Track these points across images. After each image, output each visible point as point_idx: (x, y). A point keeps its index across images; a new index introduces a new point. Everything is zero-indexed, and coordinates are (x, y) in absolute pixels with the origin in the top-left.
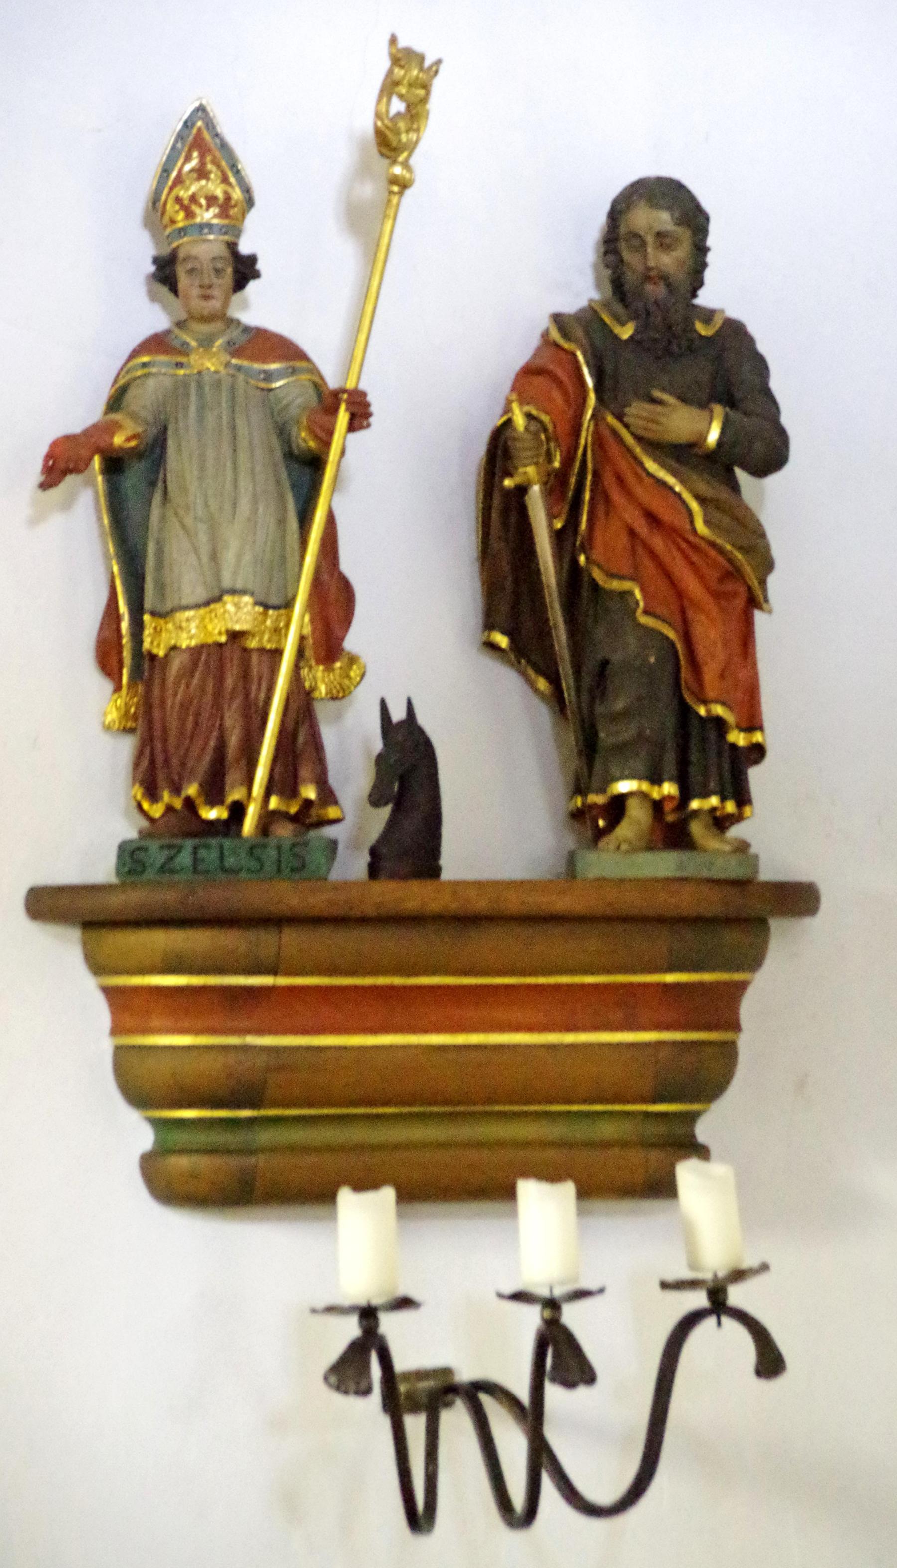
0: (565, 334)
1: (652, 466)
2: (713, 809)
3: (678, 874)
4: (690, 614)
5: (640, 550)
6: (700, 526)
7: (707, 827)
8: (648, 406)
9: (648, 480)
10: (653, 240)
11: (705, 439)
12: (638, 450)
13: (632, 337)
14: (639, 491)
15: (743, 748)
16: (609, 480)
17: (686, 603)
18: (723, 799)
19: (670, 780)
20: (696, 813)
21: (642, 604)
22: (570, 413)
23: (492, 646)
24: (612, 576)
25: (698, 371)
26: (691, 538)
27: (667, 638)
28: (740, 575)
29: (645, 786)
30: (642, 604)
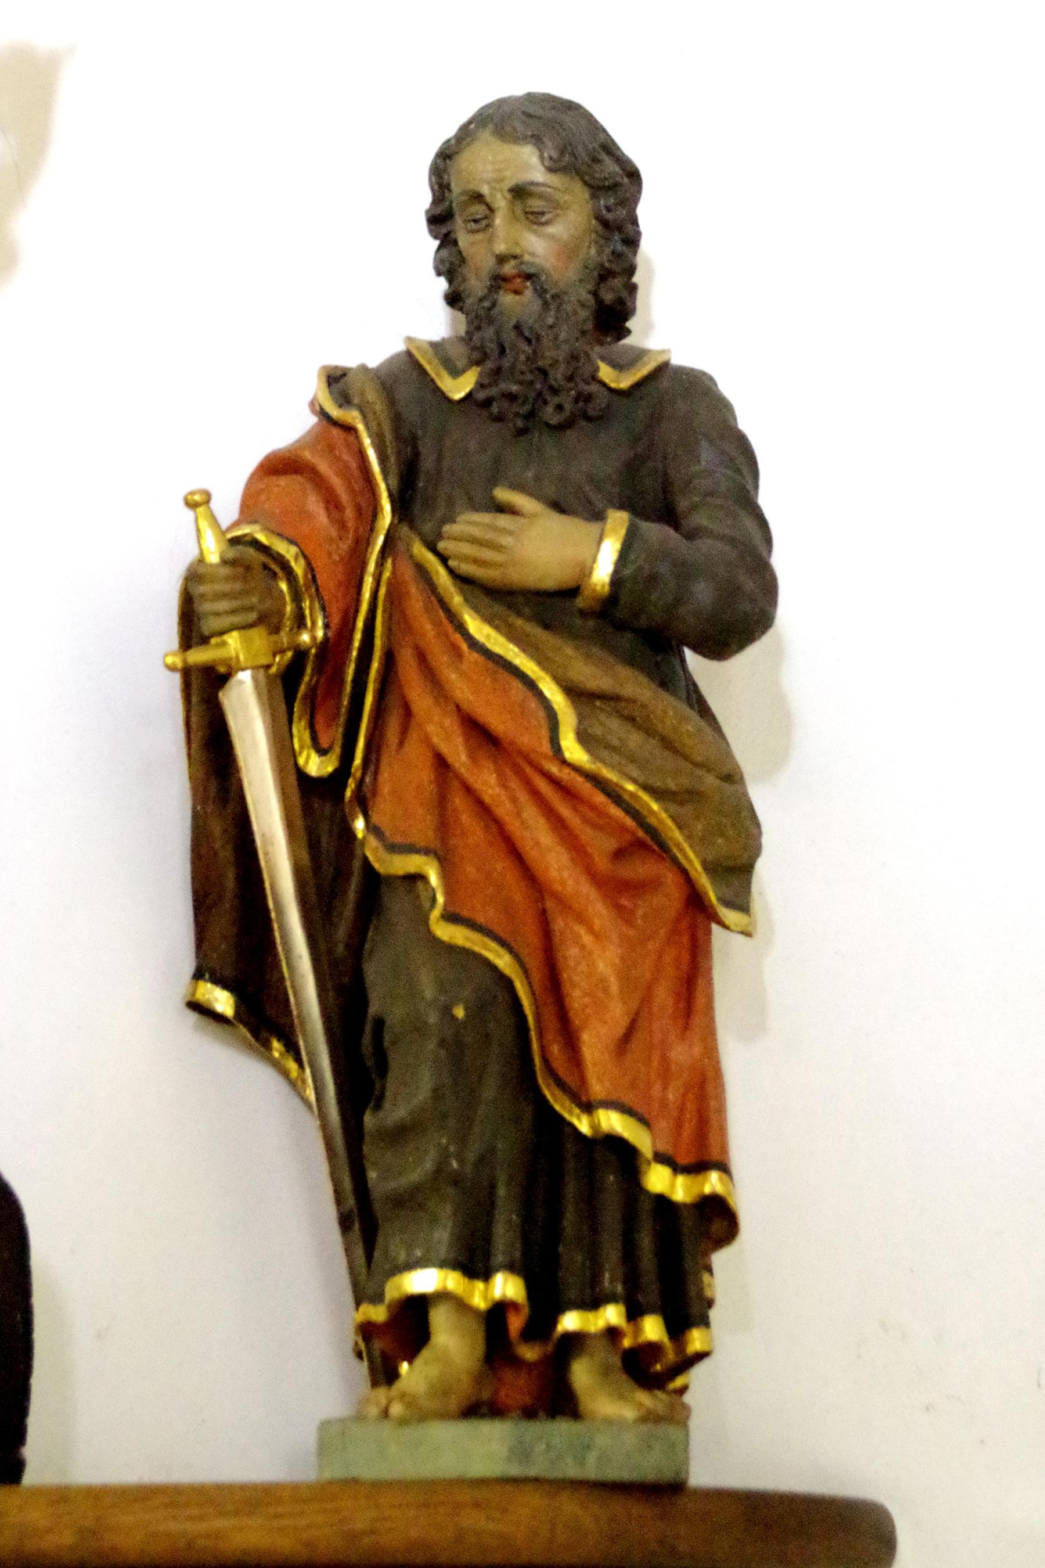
0: (344, 400)
1: (475, 626)
2: (612, 1333)
3: (514, 1470)
4: (558, 924)
5: (458, 801)
6: (573, 750)
7: (606, 1372)
8: (485, 518)
9: (472, 656)
10: (542, 239)
11: (591, 570)
12: (456, 600)
13: (469, 395)
14: (451, 677)
15: (685, 1205)
16: (406, 659)
17: (550, 904)
18: (634, 1314)
19: (511, 1268)
20: (575, 1341)
21: (440, 899)
22: (345, 546)
23: (200, 1008)
24: (394, 848)
25: (598, 457)
26: (554, 769)
27: (494, 968)
28: (689, 863)
29: (452, 1281)
30: (440, 899)
